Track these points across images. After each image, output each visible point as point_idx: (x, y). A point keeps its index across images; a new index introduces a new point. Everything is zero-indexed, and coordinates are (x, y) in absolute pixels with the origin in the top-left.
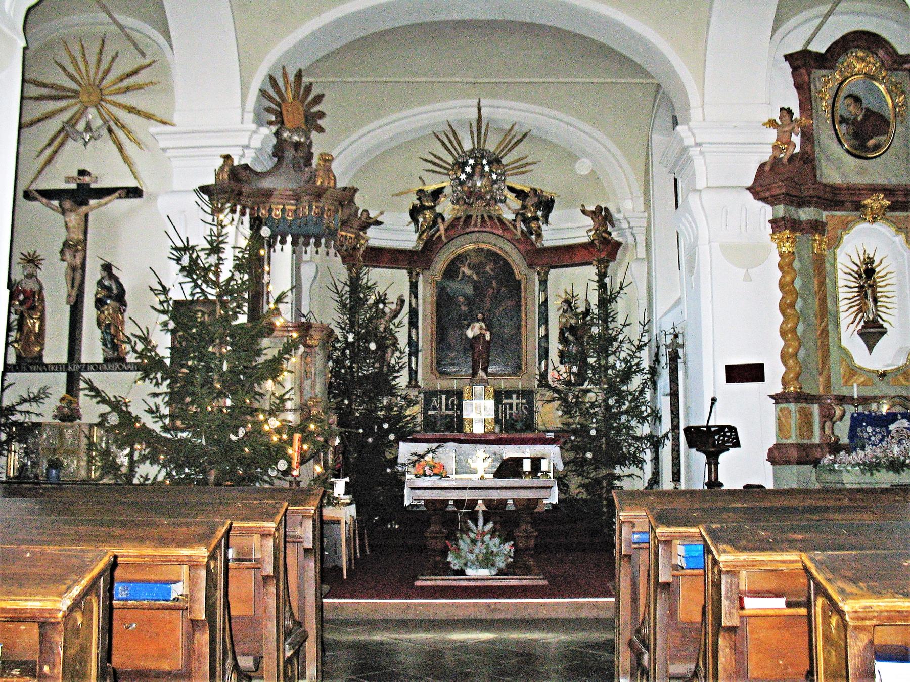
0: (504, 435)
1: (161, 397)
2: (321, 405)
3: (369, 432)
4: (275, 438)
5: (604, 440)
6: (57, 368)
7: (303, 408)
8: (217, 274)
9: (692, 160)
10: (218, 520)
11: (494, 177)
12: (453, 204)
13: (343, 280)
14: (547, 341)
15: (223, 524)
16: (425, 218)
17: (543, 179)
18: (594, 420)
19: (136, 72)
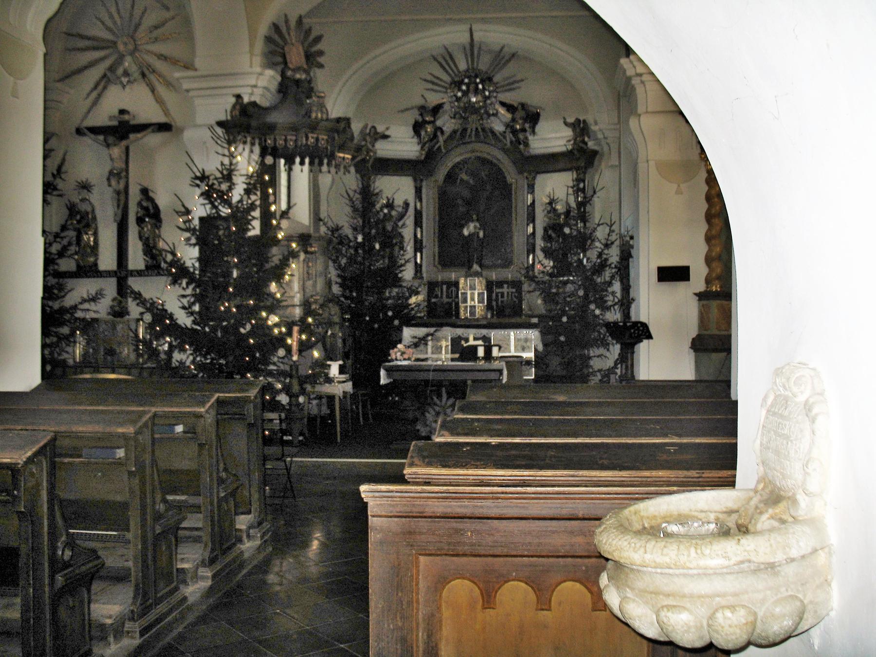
0: (495, 320)
4: (276, 331)
6: (108, 274)
11: (487, 93)
17: (532, 93)
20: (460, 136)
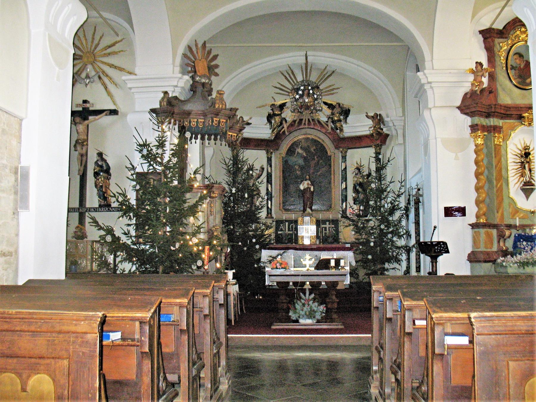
0: (322, 245)
1: (132, 226)
2: (219, 230)
3: (244, 245)
4: (195, 249)
5: (378, 248)
7: (210, 232)
8: (162, 159)
9: (426, 92)
11: (315, 96)
12: (292, 112)
13: (229, 157)
14: (346, 191)
15: (192, 289)
16: (275, 121)
17: (344, 98)
18: (373, 237)
19: (113, 45)
20: (296, 124)
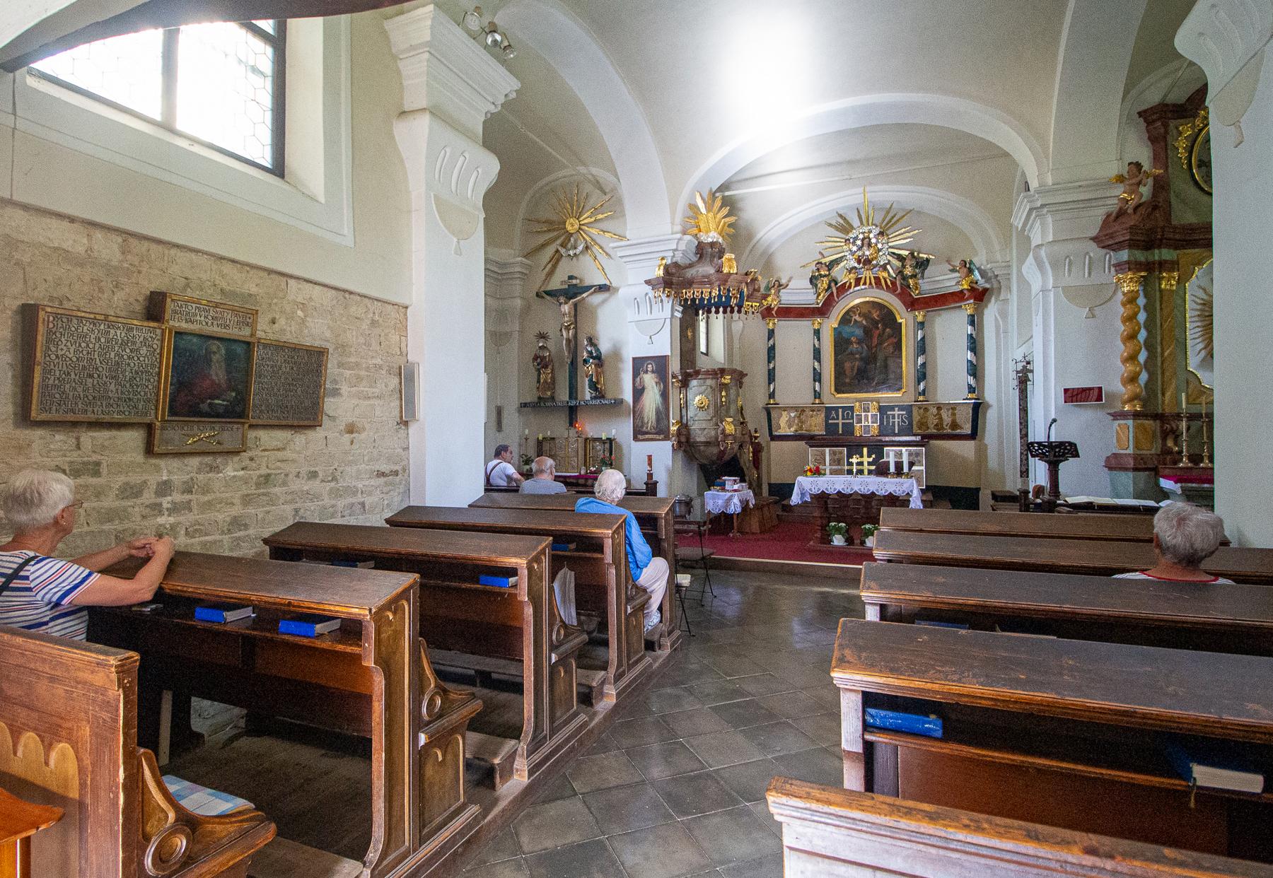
10: (867, 526)
